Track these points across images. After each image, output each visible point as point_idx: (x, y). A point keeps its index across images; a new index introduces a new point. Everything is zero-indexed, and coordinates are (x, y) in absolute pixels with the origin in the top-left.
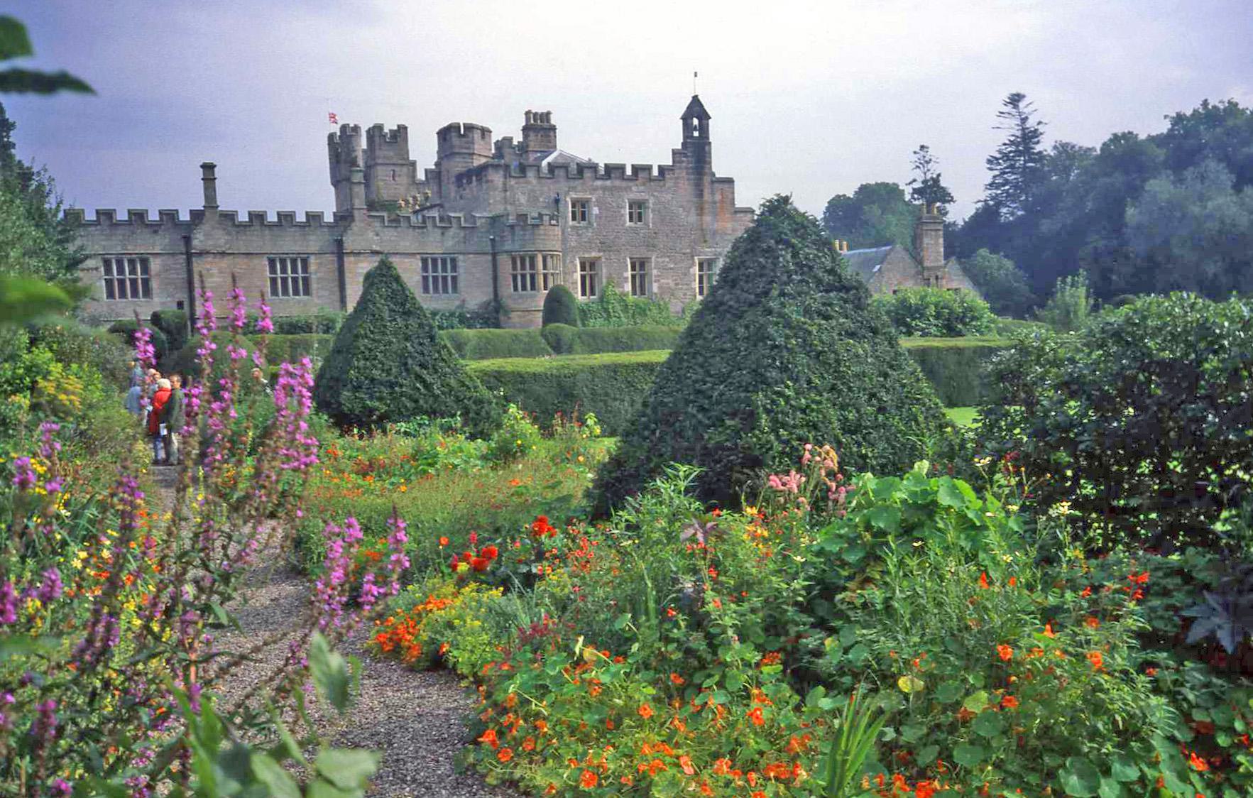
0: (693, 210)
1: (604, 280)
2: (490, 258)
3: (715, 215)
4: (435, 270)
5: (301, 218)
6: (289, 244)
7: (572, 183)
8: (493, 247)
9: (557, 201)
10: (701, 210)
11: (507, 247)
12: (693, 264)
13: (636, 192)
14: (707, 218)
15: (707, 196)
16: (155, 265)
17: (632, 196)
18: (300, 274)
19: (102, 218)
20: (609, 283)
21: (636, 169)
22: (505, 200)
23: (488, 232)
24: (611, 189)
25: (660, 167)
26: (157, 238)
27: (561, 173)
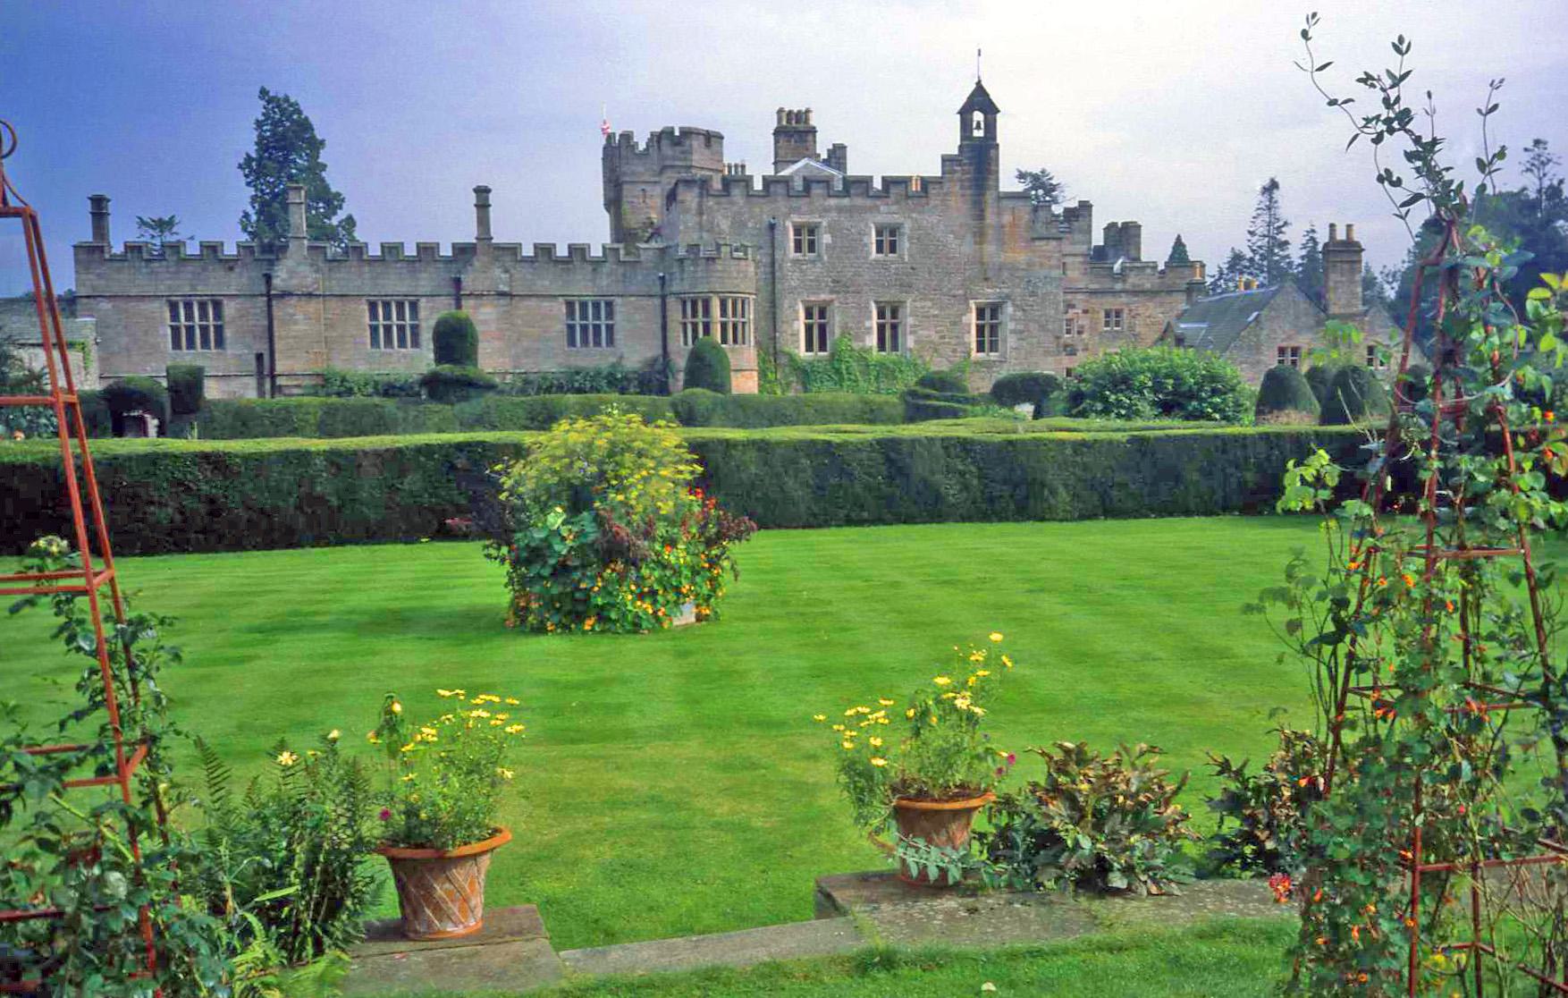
0: (969, 238)
1: (837, 331)
2: (657, 301)
3: (1001, 243)
4: (584, 316)
5: (410, 251)
6: (395, 283)
7: (795, 203)
8: (663, 285)
9: (772, 227)
10: (980, 236)
11: (675, 288)
12: (968, 310)
13: (887, 214)
14: (990, 248)
15: (990, 219)
16: (230, 309)
17: (880, 219)
18: (408, 321)
19: (168, 252)
20: (843, 334)
21: (888, 182)
22: (701, 227)
23: (656, 268)
24: (850, 210)
25: (884, 179)
26: (233, 275)
27: (780, 189)
